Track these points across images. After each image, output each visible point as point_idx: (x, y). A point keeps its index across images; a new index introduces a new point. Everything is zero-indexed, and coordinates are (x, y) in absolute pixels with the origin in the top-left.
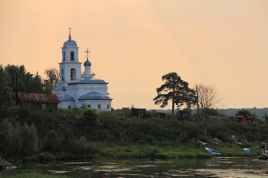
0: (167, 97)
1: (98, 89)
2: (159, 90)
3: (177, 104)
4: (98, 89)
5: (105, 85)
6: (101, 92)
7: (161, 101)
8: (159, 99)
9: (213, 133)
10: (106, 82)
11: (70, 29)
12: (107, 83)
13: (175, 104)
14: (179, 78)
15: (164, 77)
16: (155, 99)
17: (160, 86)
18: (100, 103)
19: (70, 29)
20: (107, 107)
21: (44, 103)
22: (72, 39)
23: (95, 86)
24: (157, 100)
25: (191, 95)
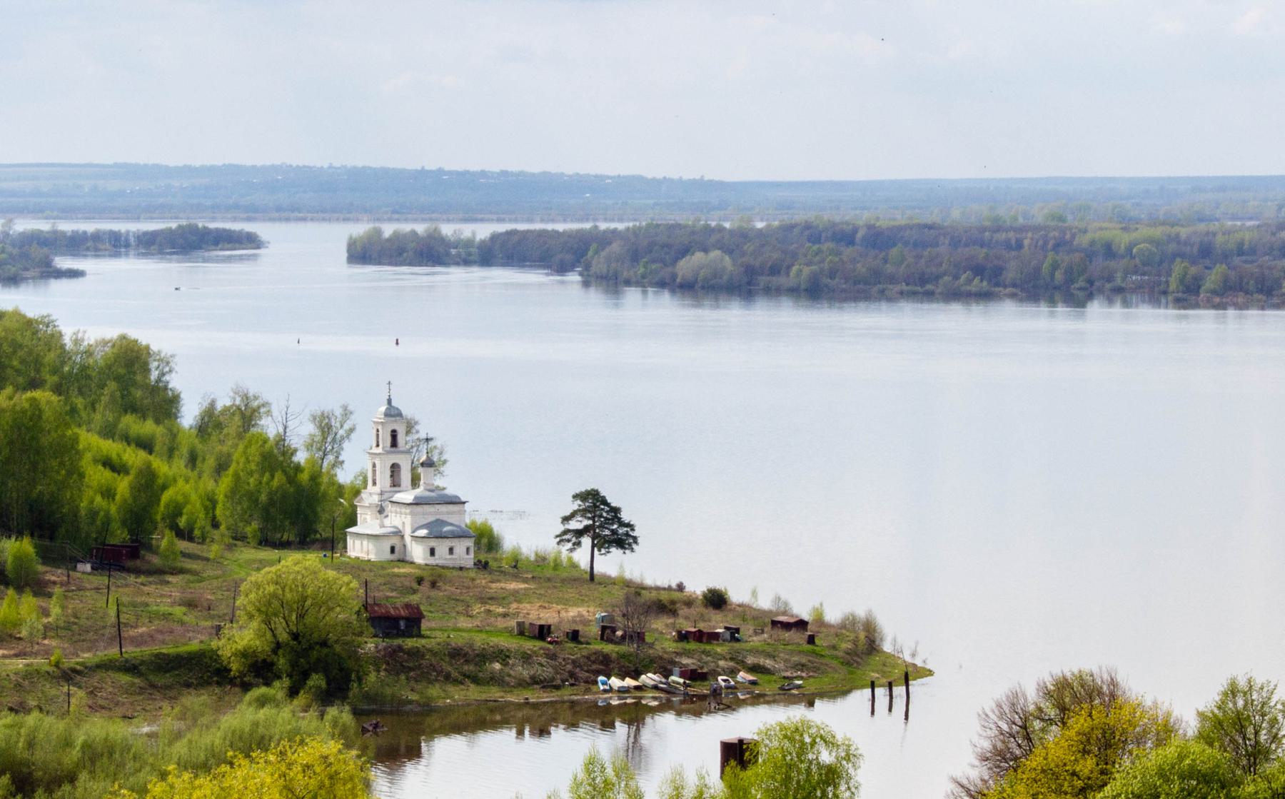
0: (579, 533)
1: (448, 513)
2: (566, 519)
3: (599, 550)
4: (448, 513)
5: (461, 506)
6: (453, 519)
7: (569, 541)
8: (564, 537)
9: (787, 657)
10: (463, 499)
11: (389, 383)
12: (464, 503)
13: (596, 549)
14: (605, 502)
15: (576, 497)
16: (557, 536)
17: (568, 514)
18: (453, 544)
19: (389, 383)
20: (465, 550)
21: (403, 618)
22: (394, 404)
23: (444, 508)
24: (562, 538)
25: (627, 534)
